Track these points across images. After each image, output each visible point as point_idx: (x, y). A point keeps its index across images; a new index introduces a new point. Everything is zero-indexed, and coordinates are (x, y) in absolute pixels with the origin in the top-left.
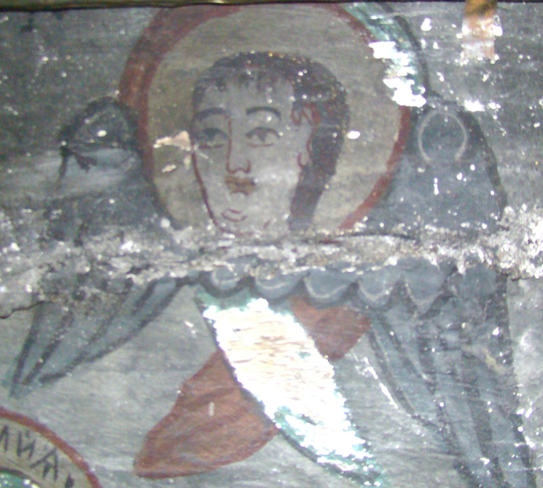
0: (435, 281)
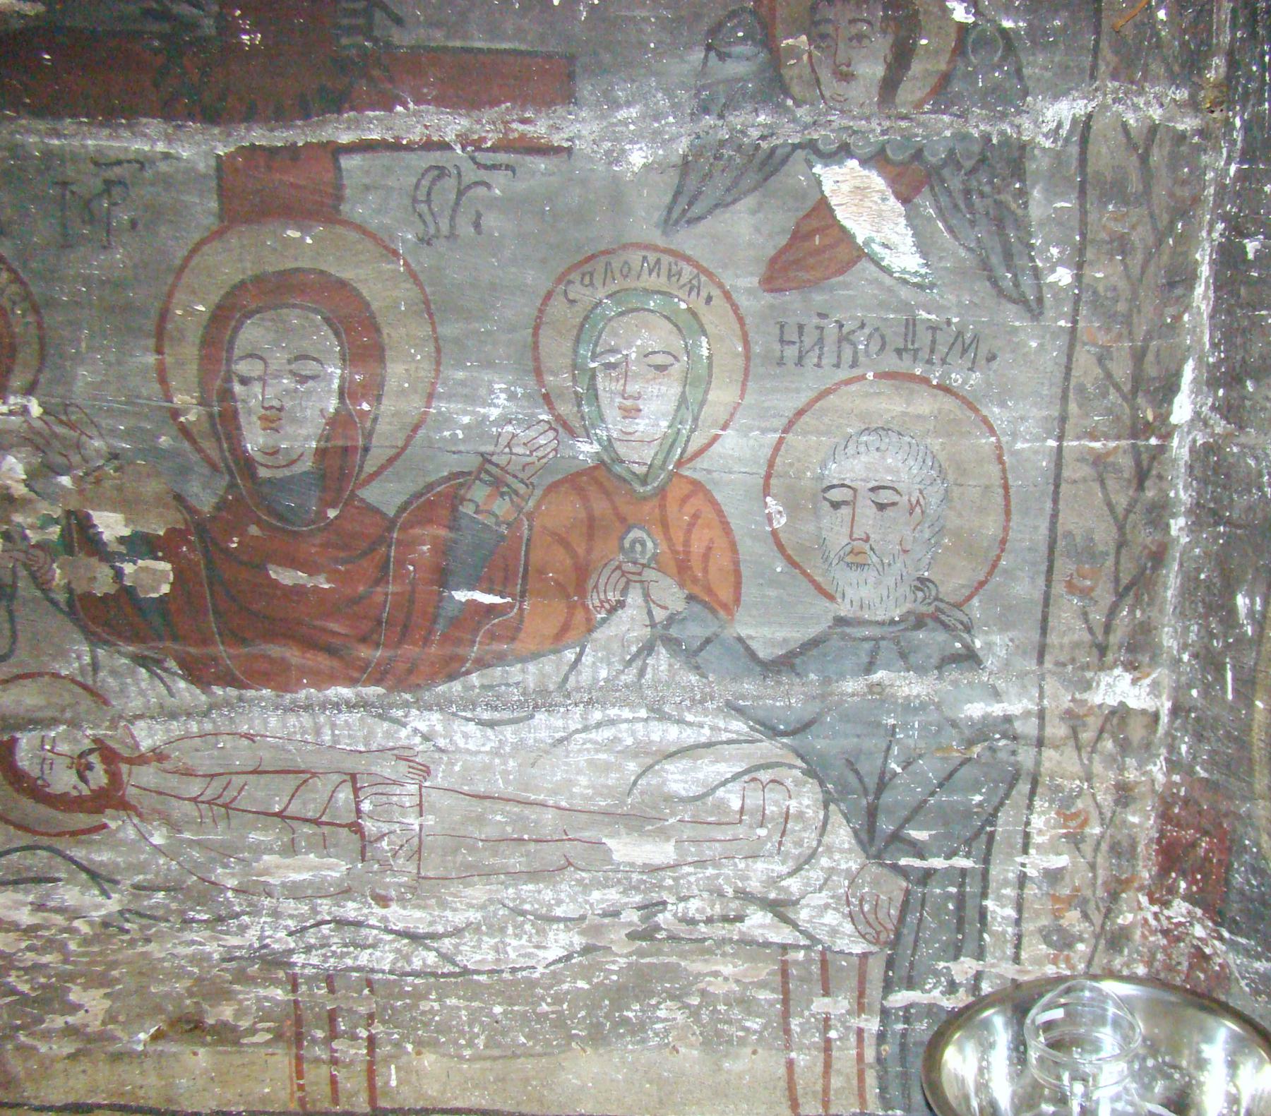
0: (976, 148)
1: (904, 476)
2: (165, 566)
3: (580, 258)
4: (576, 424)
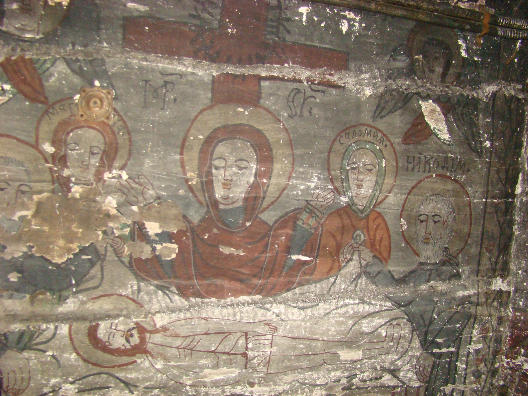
1: (443, 211)
2: (175, 246)
3: (345, 128)
4: (340, 190)
